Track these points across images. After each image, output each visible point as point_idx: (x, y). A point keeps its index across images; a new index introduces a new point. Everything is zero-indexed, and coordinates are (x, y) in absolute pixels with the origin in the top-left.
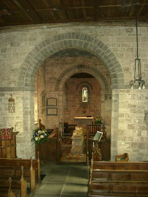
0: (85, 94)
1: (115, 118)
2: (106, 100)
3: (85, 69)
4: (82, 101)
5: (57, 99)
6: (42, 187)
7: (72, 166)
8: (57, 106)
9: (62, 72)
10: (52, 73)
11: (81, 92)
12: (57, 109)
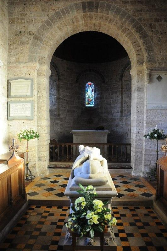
0: (90, 93)
4: (85, 104)
10: (23, 21)
12: (32, 105)
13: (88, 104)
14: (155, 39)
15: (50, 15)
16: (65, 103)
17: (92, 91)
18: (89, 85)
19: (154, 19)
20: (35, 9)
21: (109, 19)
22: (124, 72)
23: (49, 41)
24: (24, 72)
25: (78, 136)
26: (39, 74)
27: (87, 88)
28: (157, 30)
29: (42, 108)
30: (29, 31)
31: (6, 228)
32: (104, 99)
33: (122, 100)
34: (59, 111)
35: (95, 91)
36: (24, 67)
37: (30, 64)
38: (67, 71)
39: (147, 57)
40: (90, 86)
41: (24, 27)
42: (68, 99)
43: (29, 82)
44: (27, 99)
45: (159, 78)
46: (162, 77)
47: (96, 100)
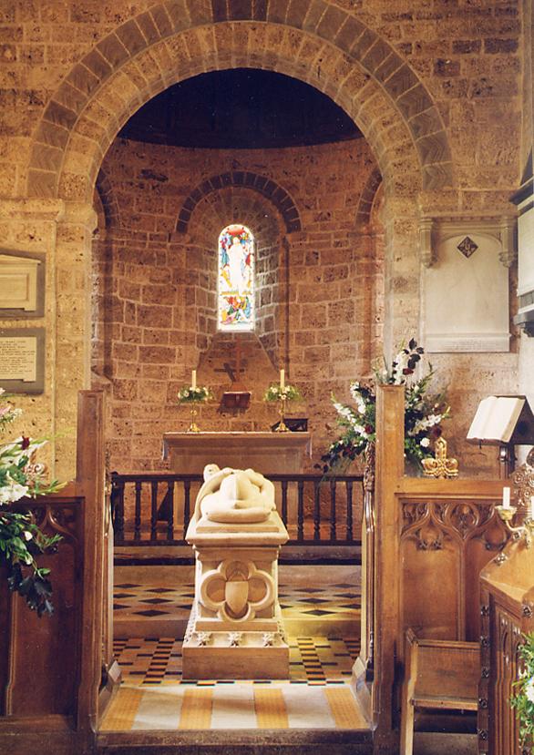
1: (269, 742)
2: (435, 260)
3: (272, 29)
4: (213, 324)
5: (41, 258)
6: (340, 56)
7: (439, 339)
8: (40, 313)
9: (87, 47)
11: (205, 255)
14: (457, 110)
15: (104, 36)
16: (133, 318)
17: (248, 261)
18: (234, 234)
19: (451, 44)
20: (50, 12)
21: (302, 44)
22: (375, 188)
23: (100, 124)
24: (14, 231)
25: (191, 453)
26: (63, 233)
27: (224, 248)
28: (462, 82)
29: (74, 354)
30: (29, 88)
31: (525, 11)
32: (296, 302)
34: (108, 355)
36: (12, 214)
37: (34, 206)
38: (142, 186)
39: (427, 174)
41: (12, 75)
42: (145, 300)
43: (30, 268)
44: (23, 323)
45: (468, 248)
46: (475, 239)
47: (263, 304)
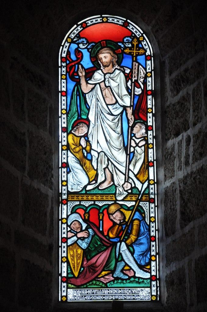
4: (50, 278)
13: (88, 276)
17: (139, 111)
18: (97, 45)
33: (162, 100)
35: (165, 112)
40: (105, 56)
